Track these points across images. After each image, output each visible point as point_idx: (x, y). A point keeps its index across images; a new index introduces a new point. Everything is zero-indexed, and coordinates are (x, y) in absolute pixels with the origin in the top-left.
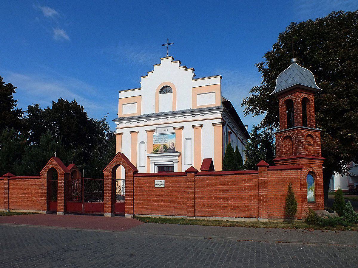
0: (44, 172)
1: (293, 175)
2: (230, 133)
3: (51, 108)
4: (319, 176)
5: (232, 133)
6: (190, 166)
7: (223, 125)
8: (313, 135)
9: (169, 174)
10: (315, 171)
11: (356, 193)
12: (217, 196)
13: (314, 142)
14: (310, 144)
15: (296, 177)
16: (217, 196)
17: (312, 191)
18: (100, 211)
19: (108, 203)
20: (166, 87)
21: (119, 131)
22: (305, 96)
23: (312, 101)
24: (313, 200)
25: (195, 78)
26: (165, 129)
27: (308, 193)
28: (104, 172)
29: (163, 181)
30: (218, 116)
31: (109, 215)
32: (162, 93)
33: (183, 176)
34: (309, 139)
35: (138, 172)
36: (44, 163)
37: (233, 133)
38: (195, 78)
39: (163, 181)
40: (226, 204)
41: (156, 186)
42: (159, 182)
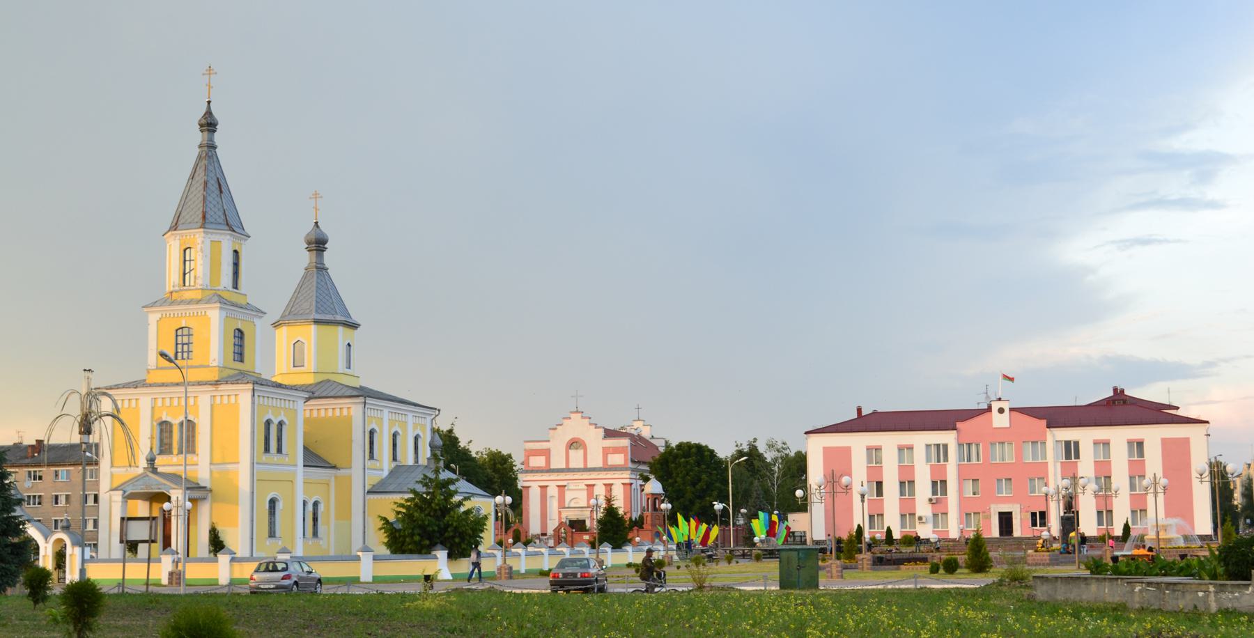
32: (572, 447)
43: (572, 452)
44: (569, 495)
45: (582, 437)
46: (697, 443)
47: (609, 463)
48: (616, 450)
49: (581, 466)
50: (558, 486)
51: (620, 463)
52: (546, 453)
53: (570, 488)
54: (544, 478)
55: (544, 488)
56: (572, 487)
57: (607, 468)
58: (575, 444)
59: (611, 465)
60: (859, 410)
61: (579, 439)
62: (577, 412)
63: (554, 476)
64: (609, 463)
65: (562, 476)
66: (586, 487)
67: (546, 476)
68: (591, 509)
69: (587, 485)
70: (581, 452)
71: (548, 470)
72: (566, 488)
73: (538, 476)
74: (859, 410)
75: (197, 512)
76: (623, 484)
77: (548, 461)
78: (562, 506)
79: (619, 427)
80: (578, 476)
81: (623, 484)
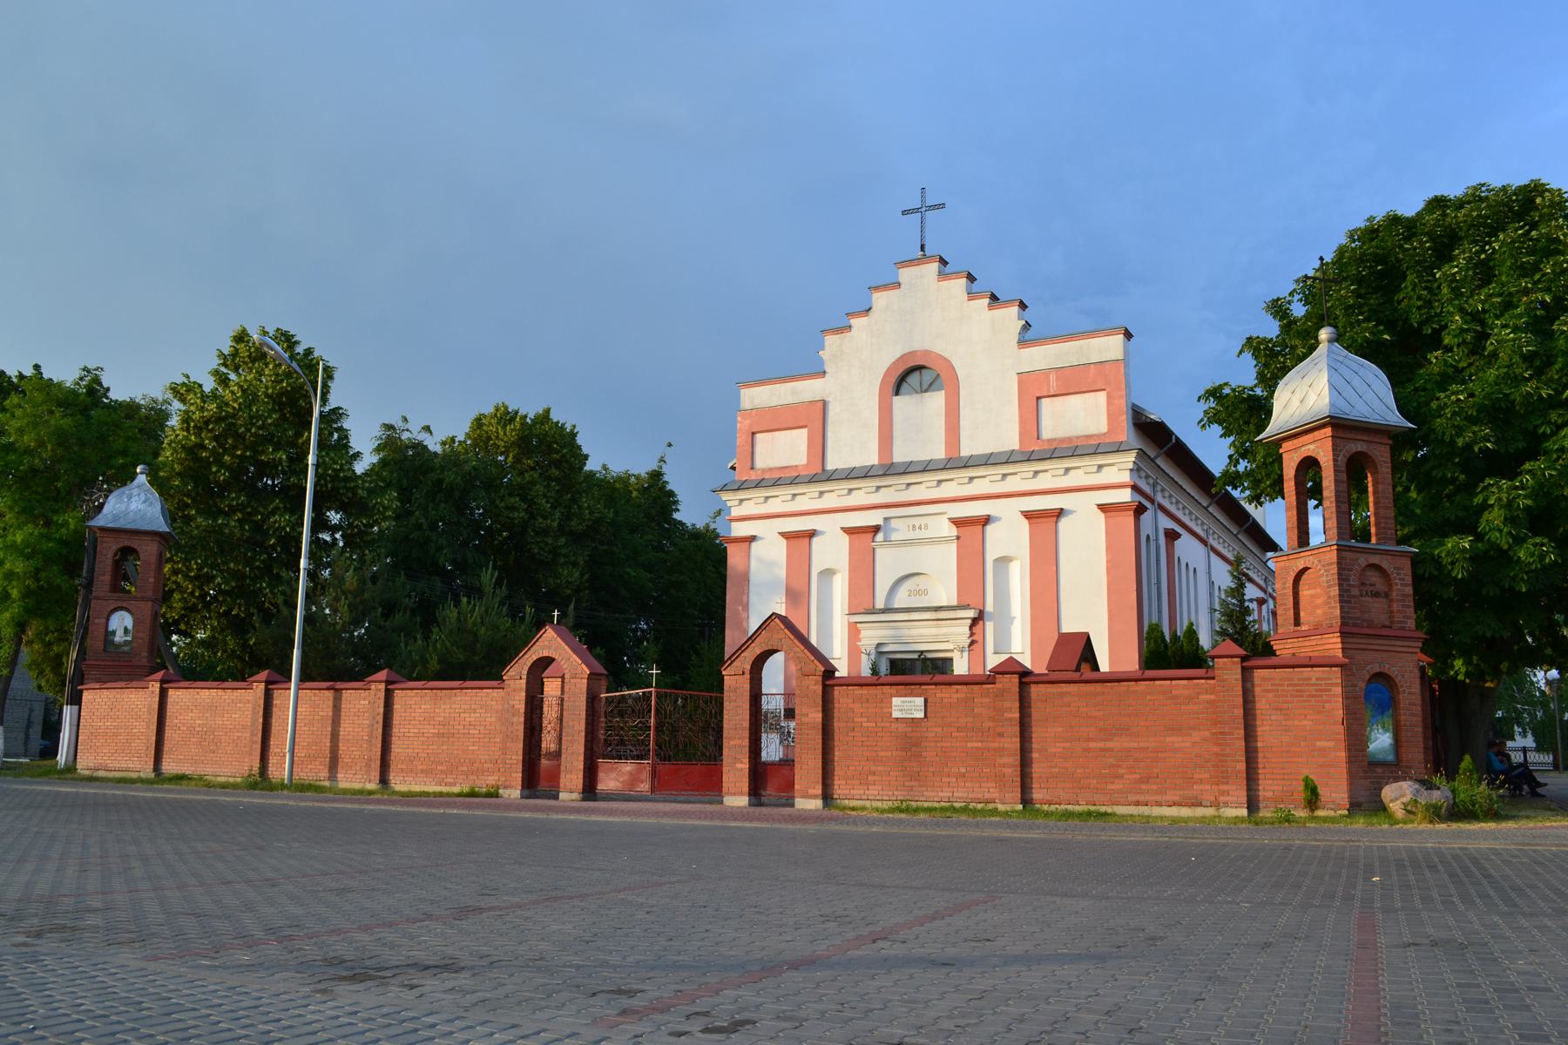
0: (517, 674)
1: (1321, 685)
2: (1172, 536)
3: (676, 516)
4: (1409, 687)
5: (1178, 536)
6: (1007, 656)
7: (1139, 510)
8: (1385, 565)
9: (938, 678)
10: (1394, 671)
11: (318, 488)
12: (1092, 745)
13: (1390, 586)
14: (1376, 595)
15: (1330, 691)
16: (1092, 745)
17: (1386, 730)
18: (712, 785)
19: (735, 769)
20: (920, 368)
21: (739, 530)
22: (1360, 447)
23: (1385, 462)
24: (1391, 757)
25: (1027, 335)
26: (917, 522)
27: (1373, 737)
28: (724, 673)
29: (920, 701)
30: (1119, 470)
31: (742, 801)
32: (905, 387)
33: (982, 684)
34: (1374, 578)
35: (837, 674)
36: (525, 642)
37: (1185, 536)
38: (1027, 335)
39: (920, 701)
40: (1120, 766)
41: (896, 714)
42: (905, 704)
43: (903, 405)
44: (888, 564)
45: (940, 347)
46: (530, 409)
47: (1046, 434)
48: (1073, 382)
49: (871, 458)
50: (849, 531)
51: (1093, 430)
52: (815, 417)
53: (894, 536)
54: (1045, 482)
55: (1045, 521)
56: (900, 530)
57: (1038, 452)
58: (914, 379)
59: (1050, 441)
60: (1321, 259)
61: (927, 353)
62: (924, 259)
63: (835, 496)
64: (1046, 434)
65: (864, 494)
66: (954, 531)
67: (808, 498)
68: (971, 614)
69: (958, 523)
70: (936, 401)
71: (820, 475)
72: (880, 537)
73: (780, 501)
74: (1321, 259)
75: (832, 581)
76: (783, 534)
77: (819, 446)
78: (863, 605)
79: (94, 367)
80: (925, 488)
81: (783, 534)
